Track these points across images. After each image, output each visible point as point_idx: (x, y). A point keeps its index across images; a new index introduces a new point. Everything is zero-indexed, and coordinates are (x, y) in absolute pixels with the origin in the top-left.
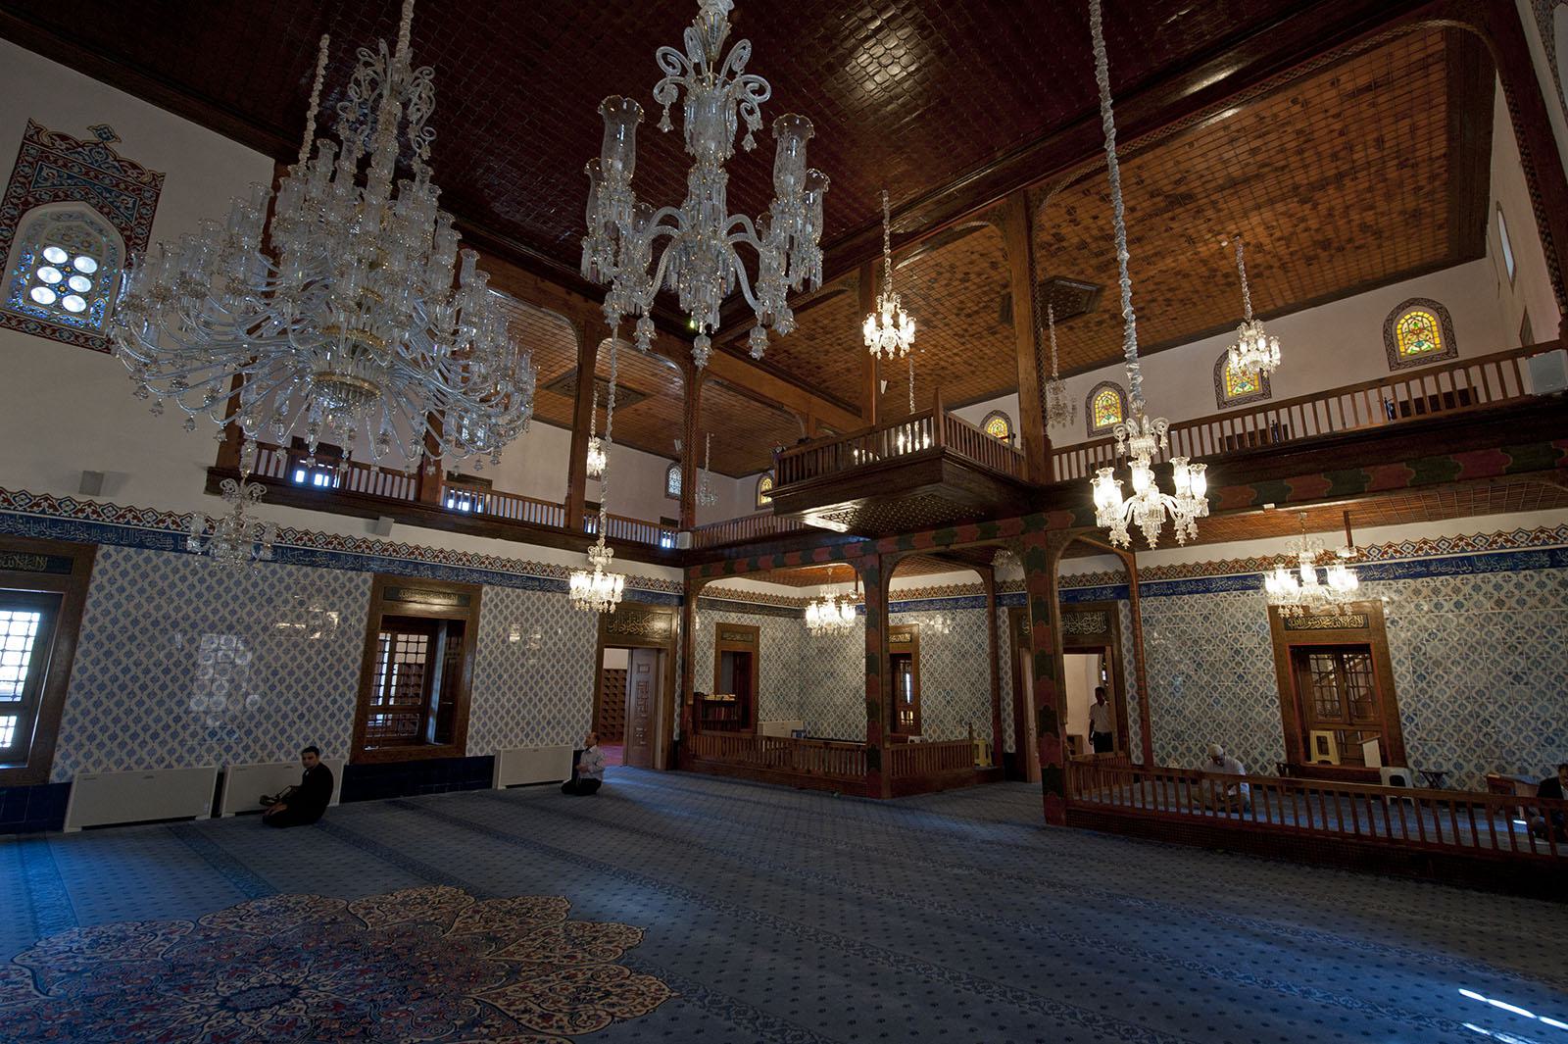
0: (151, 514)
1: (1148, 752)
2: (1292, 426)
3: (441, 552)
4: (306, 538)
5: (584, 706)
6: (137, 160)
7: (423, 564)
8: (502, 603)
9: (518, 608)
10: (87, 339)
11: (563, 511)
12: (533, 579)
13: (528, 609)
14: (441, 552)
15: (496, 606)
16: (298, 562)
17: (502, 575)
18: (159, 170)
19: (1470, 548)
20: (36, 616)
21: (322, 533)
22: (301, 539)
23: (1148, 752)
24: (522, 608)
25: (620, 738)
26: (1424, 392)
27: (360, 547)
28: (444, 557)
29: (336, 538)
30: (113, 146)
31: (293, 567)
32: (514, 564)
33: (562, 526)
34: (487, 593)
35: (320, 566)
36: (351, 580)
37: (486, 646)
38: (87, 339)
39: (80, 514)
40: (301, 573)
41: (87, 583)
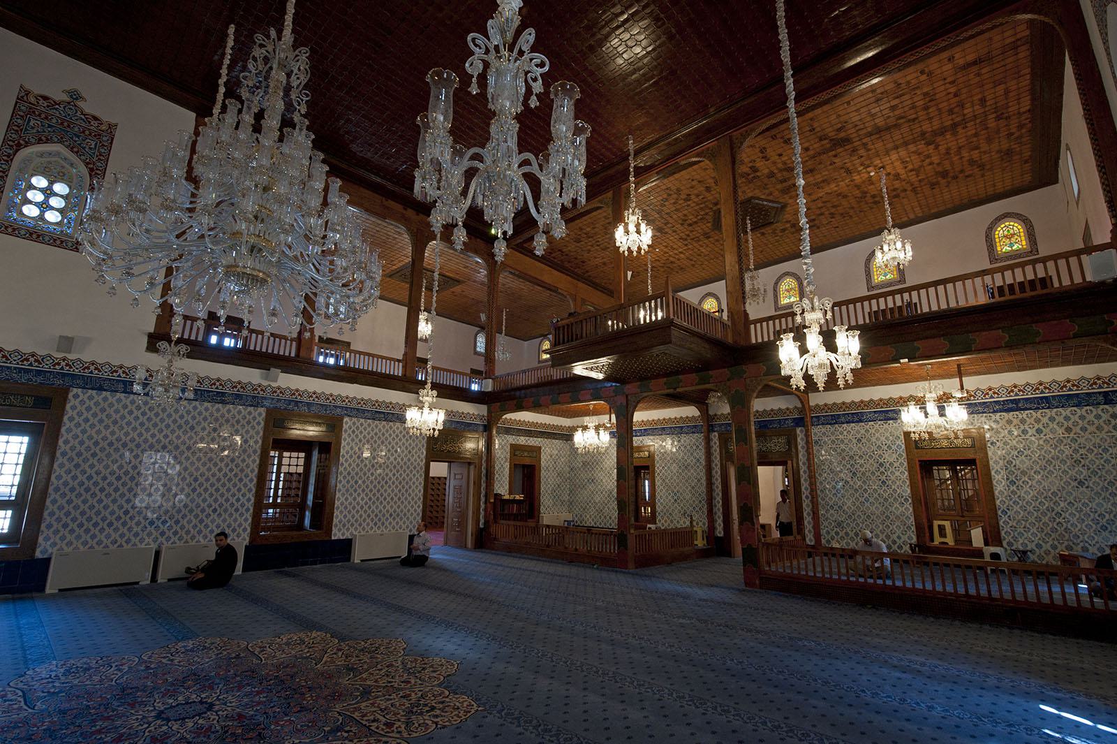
0: (107, 366)
1: (818, 536)
2: (920, 304)
3: (314, 393)
4: (218, 384)
5: (416, 503)
6: (97, 114)
7: (302, 402)
8: (358, 430)
9: (369, 433)
10: (62, 242)
11: (401, 364)
12: (380, 412)
13: (376, 434)
14: (314, 393)
15: (353, 432)
16: (212, 401)
17: (358, 409)
18: (113, 121)
19: (1047, 391)
20: (26, 439)
21: (229, 380)
22: (214, 384)
23: (818, 536)
24: (372, 434)
25: (442, 526)
26: (1014, 279)
27: (256, 389)
28: (317, 397)
29: (239, 384)
30: (80, 104)
31: (209, 404)
32: (366, 402)
33: (400, 375)
34: (347, 423)
35: (228, 403)
36: (250, 413)
37: (346, 460)
38: (62, 242)
39: (57, 367)
40: (215, 408)
41: (62, 416)
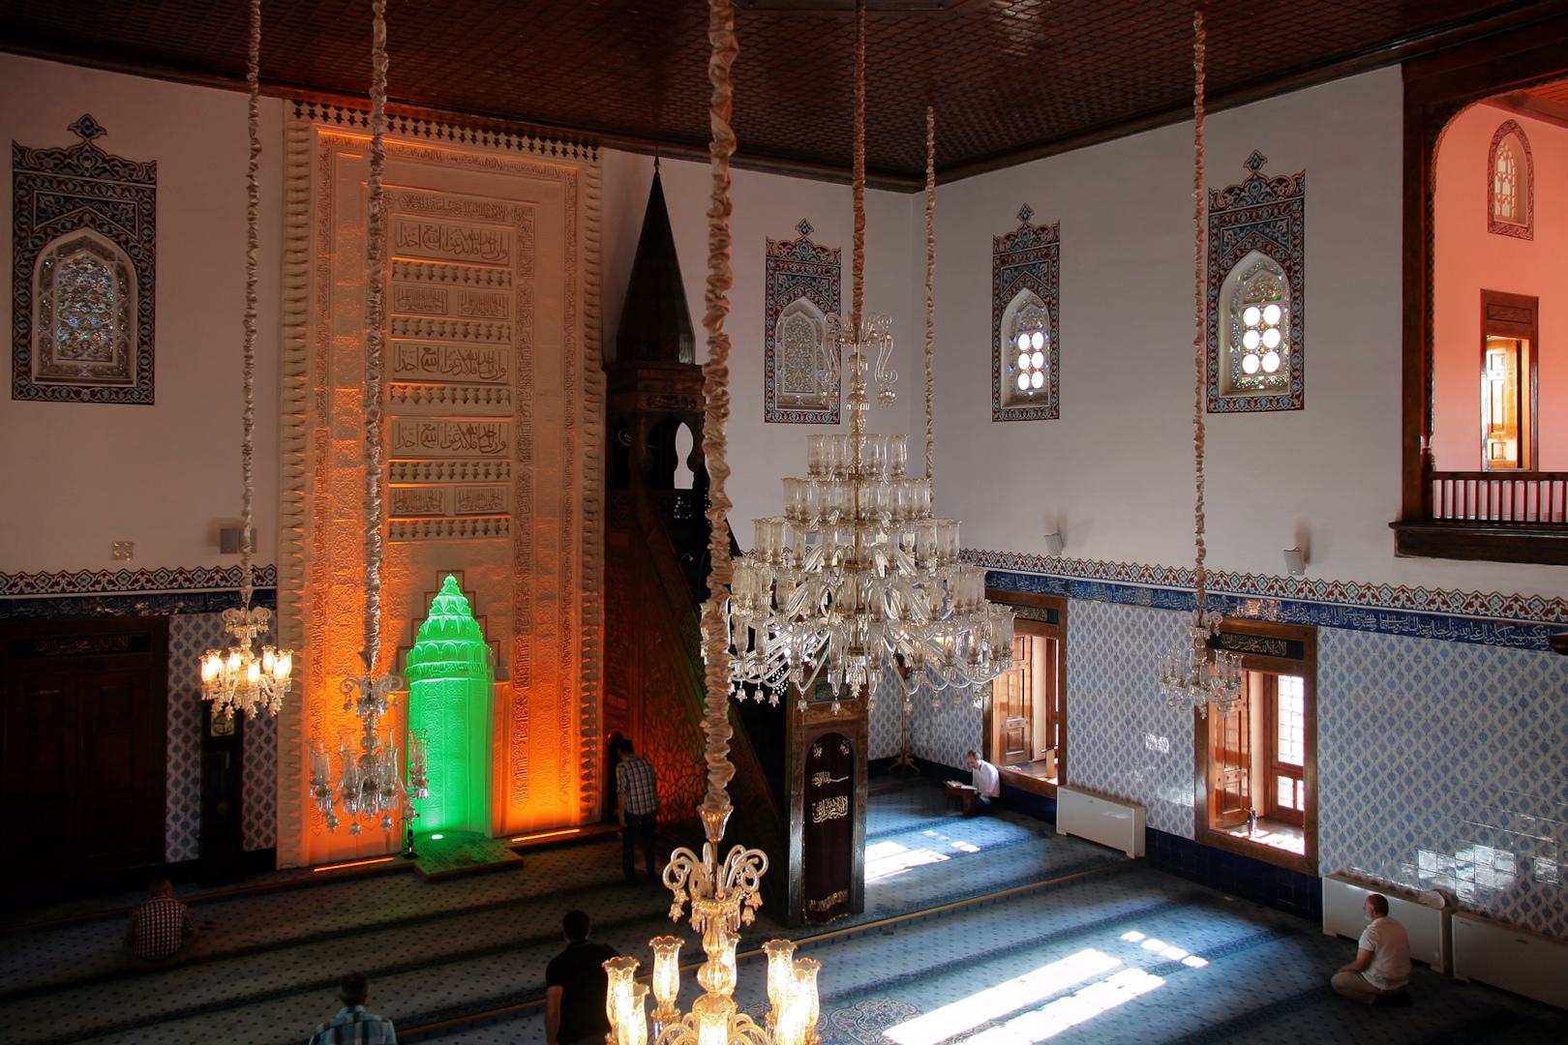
1: (1295, 786)
2: (859, 256)
4: (1516, 606)
6: (824, 244)
8: (1435, 659)
10: (144, 343)
14: (1516, 600)
16: (1511, 643)
18: (148, 160)
21: (1538, 598)
22: (1510, 608)
23: (1295, 786)
26: (723, 184)
29: (1558, 603)
30: (99, 142)
31: (1505, 650)
35: (1539, 648)
36: (1502, 661)
38: (144, 343)
40: (1538, 660)
41: (165, 798)
